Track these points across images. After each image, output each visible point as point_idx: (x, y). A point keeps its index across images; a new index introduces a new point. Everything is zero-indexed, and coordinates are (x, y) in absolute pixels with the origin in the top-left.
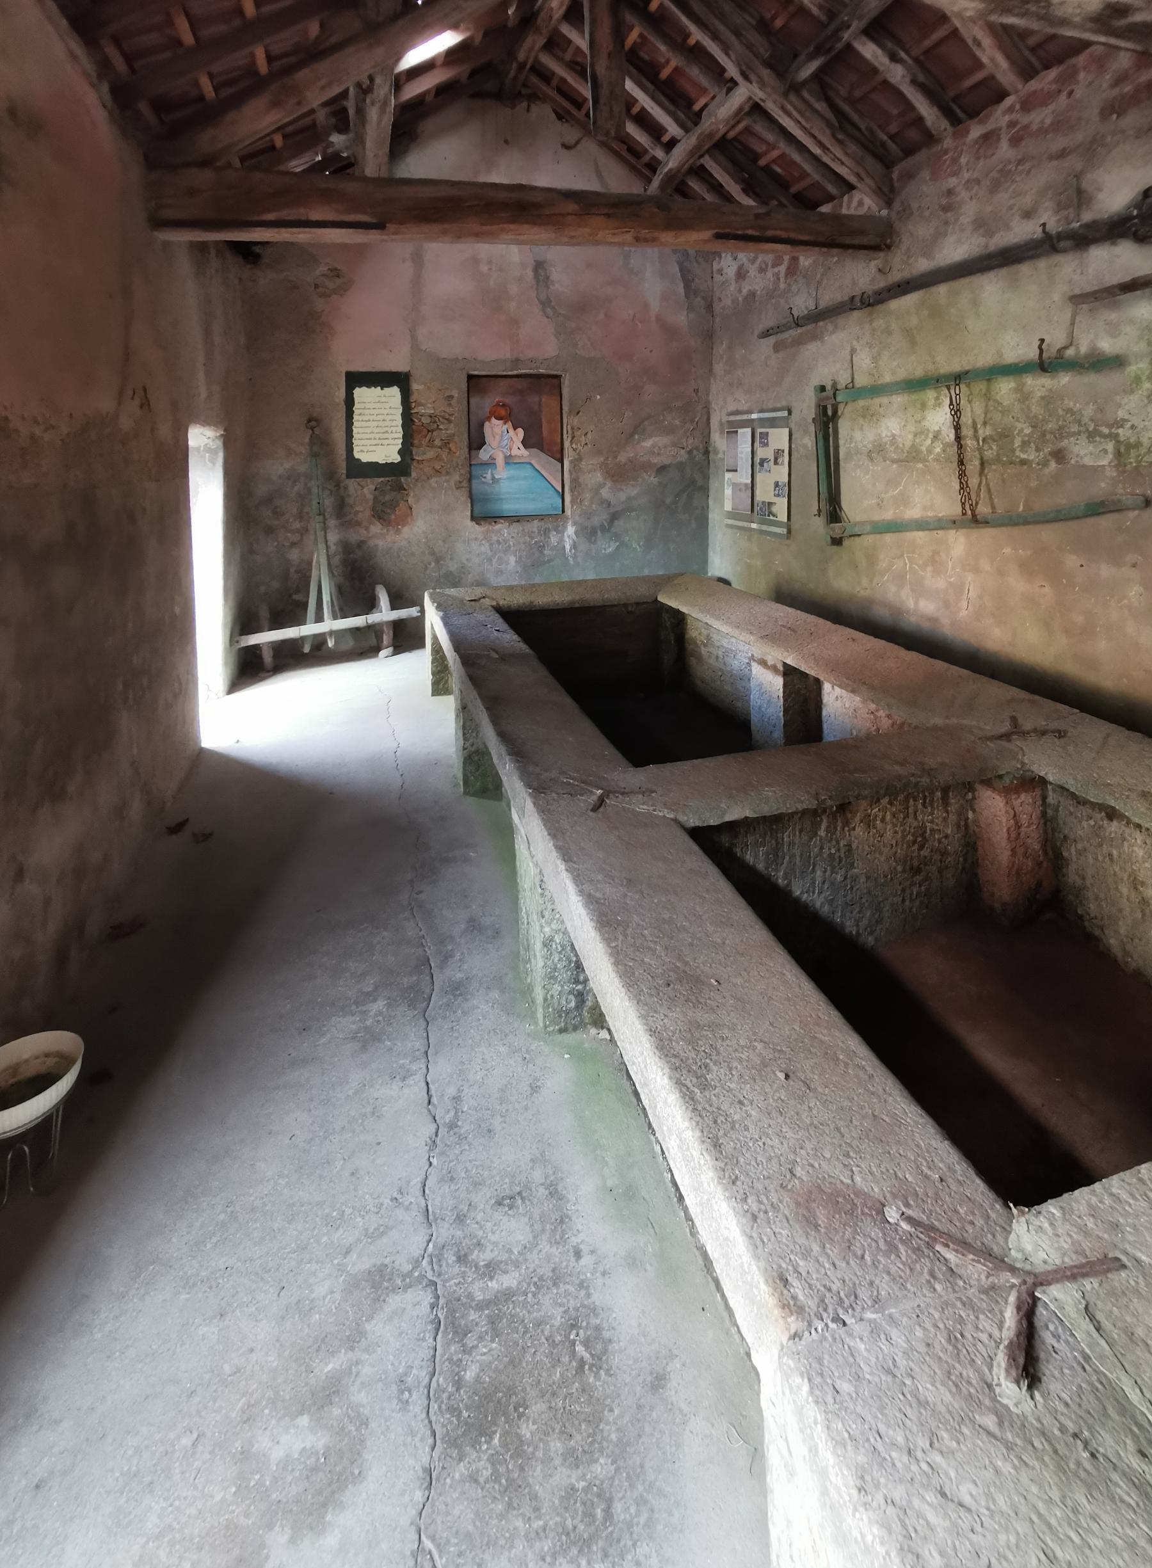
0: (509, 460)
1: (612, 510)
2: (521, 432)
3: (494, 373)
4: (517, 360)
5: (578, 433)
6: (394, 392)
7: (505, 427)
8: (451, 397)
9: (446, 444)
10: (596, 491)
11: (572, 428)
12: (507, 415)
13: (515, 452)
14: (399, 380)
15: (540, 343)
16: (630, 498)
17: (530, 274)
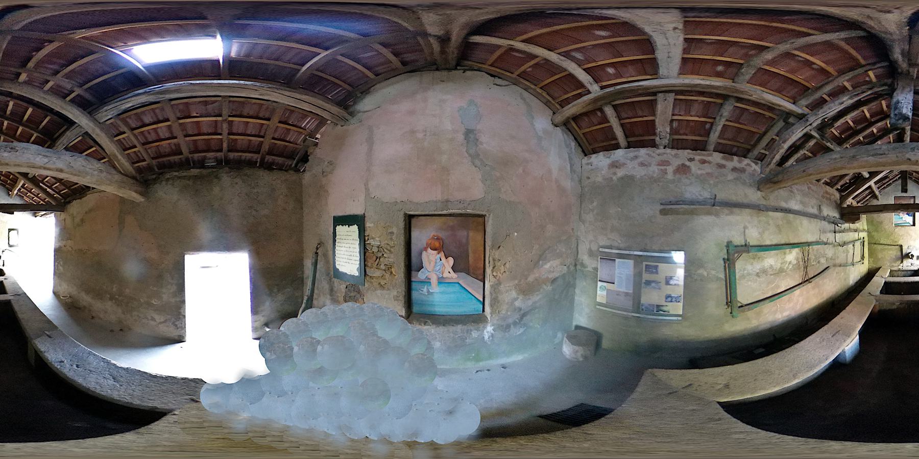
0: (441, 281)
1: (522, 312)
2: (451, 260)
3: (427, 213)
4: (447, 201)
5: (498, 264)
6: (355, 228)
7: (438, 256)
8: (392, 233)
9: (389, 268)
10: (512, 303)
11: (494, 260)
12: (440, 246)
13: (446, 275)
14: (356, 220)
15: (469, 187)
16: (535, 303)
17: (461, 137)
